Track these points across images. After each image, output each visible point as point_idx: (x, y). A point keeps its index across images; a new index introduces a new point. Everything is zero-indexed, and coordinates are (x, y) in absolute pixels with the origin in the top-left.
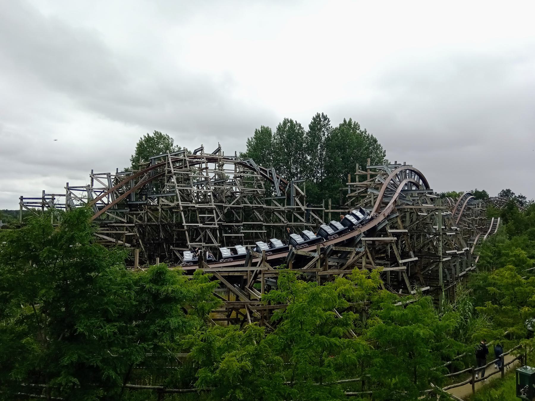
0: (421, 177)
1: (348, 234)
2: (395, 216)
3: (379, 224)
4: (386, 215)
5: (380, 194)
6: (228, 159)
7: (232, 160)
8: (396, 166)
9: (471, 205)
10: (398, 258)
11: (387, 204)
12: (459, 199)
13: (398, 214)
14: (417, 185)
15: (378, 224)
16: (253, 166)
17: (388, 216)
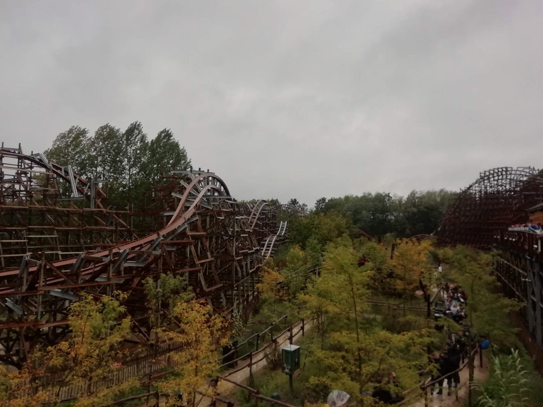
0: (222, 184)
1: (279, 337)
2: (195, 219)
3: (179, 227)
4: (187, 218)
5: (183, 198)
6: (9, 151)
7: (14, 152)
8: (200, 172)
9: (265, 210)
10: (196, 260)
11: (187, 208)
12: (256, 206)
13: (197, 218)
14: (218, 191)
15: (178, 227)
16: (43, 162)
17: (189, 219)
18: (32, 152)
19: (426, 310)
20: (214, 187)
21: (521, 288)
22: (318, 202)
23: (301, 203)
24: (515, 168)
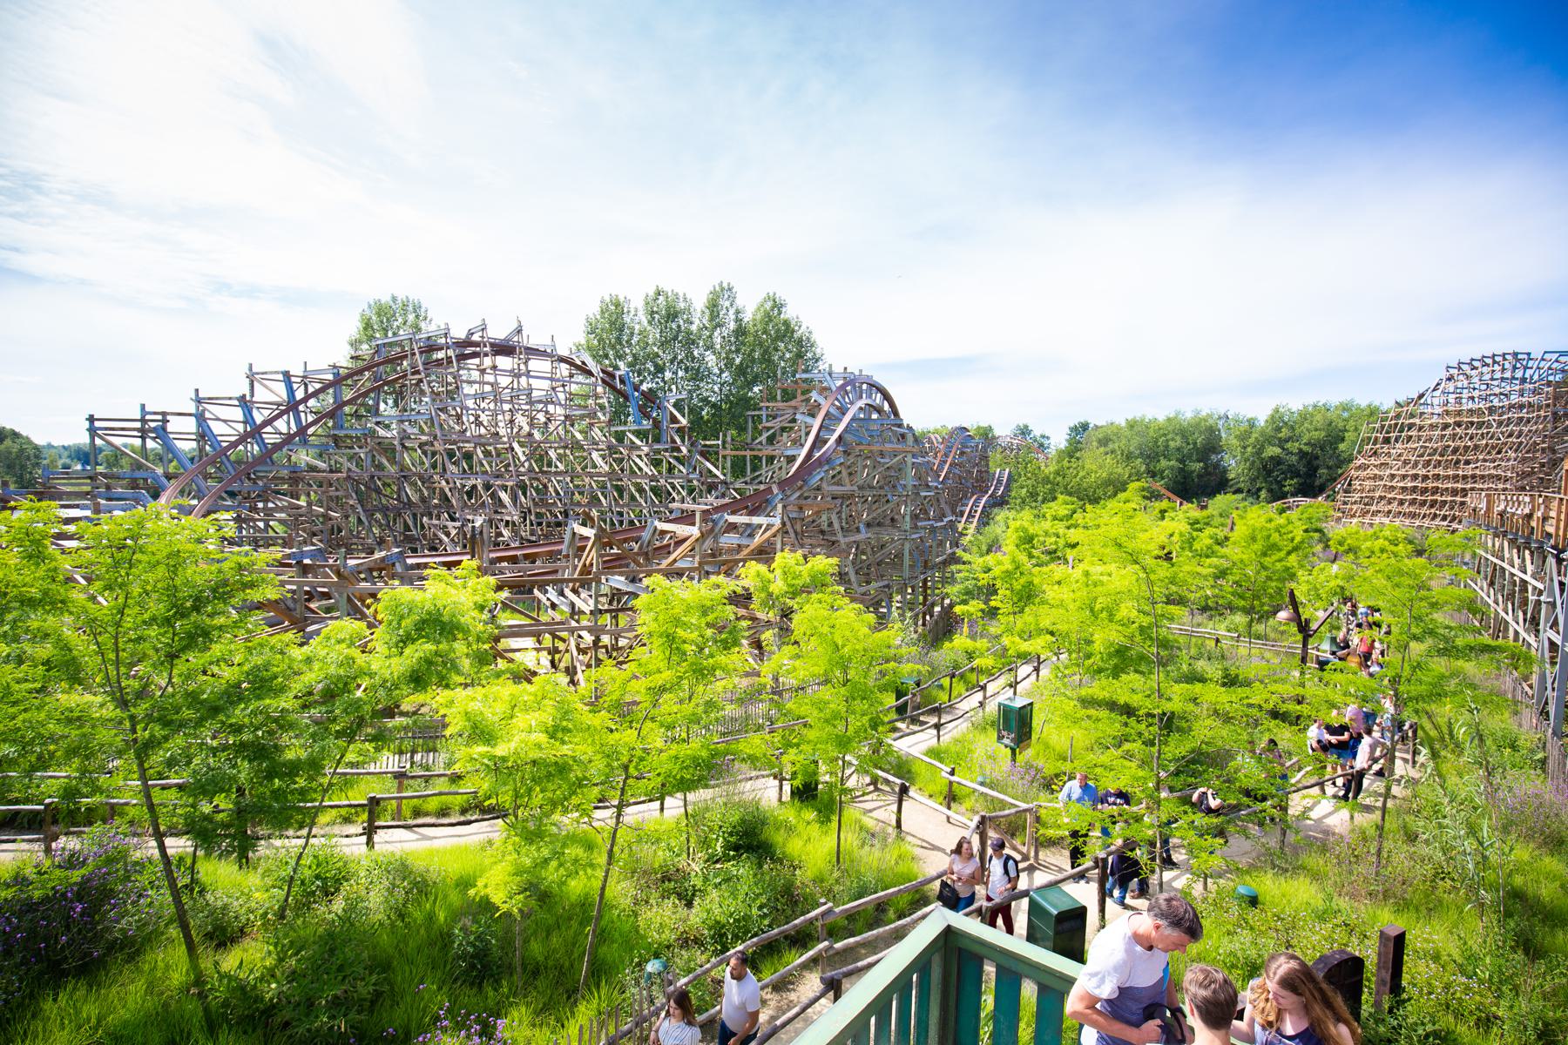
0: (886, 397)
14: (879, 410)
18: (197, 390)
19: (1299, 651)
20: (869, 402)
21: (1525, 613)
22: (1071, 429)
23: (1037, 432)
24: (1537, 354)
